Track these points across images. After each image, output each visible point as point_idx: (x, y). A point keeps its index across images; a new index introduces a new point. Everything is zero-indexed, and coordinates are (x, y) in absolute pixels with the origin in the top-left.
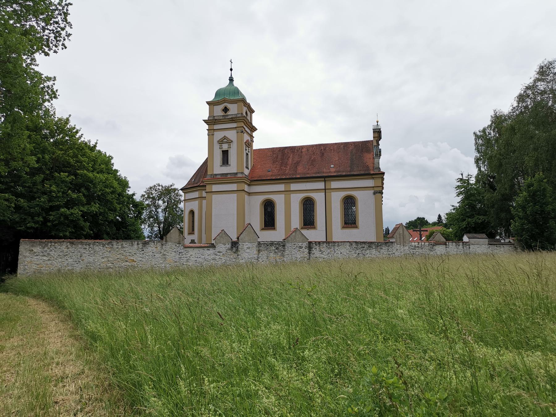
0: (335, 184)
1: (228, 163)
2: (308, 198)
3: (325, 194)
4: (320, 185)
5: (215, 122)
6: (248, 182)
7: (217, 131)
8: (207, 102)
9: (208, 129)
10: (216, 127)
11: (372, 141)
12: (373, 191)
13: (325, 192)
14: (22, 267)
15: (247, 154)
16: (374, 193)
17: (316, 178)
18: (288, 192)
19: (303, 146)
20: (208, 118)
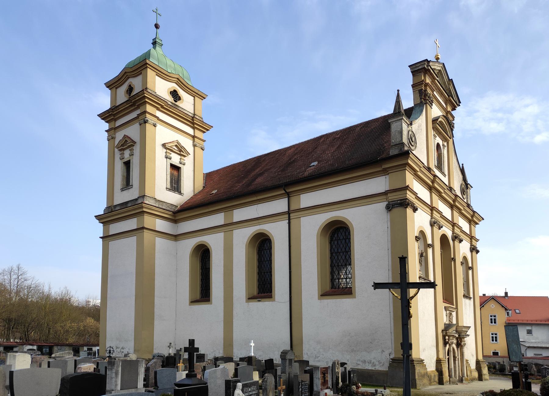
3: (289, 223)
5: (162, 107)
12: (385, 204)
13: (289, 220)
16: (389, 208)
18: (229, 226)
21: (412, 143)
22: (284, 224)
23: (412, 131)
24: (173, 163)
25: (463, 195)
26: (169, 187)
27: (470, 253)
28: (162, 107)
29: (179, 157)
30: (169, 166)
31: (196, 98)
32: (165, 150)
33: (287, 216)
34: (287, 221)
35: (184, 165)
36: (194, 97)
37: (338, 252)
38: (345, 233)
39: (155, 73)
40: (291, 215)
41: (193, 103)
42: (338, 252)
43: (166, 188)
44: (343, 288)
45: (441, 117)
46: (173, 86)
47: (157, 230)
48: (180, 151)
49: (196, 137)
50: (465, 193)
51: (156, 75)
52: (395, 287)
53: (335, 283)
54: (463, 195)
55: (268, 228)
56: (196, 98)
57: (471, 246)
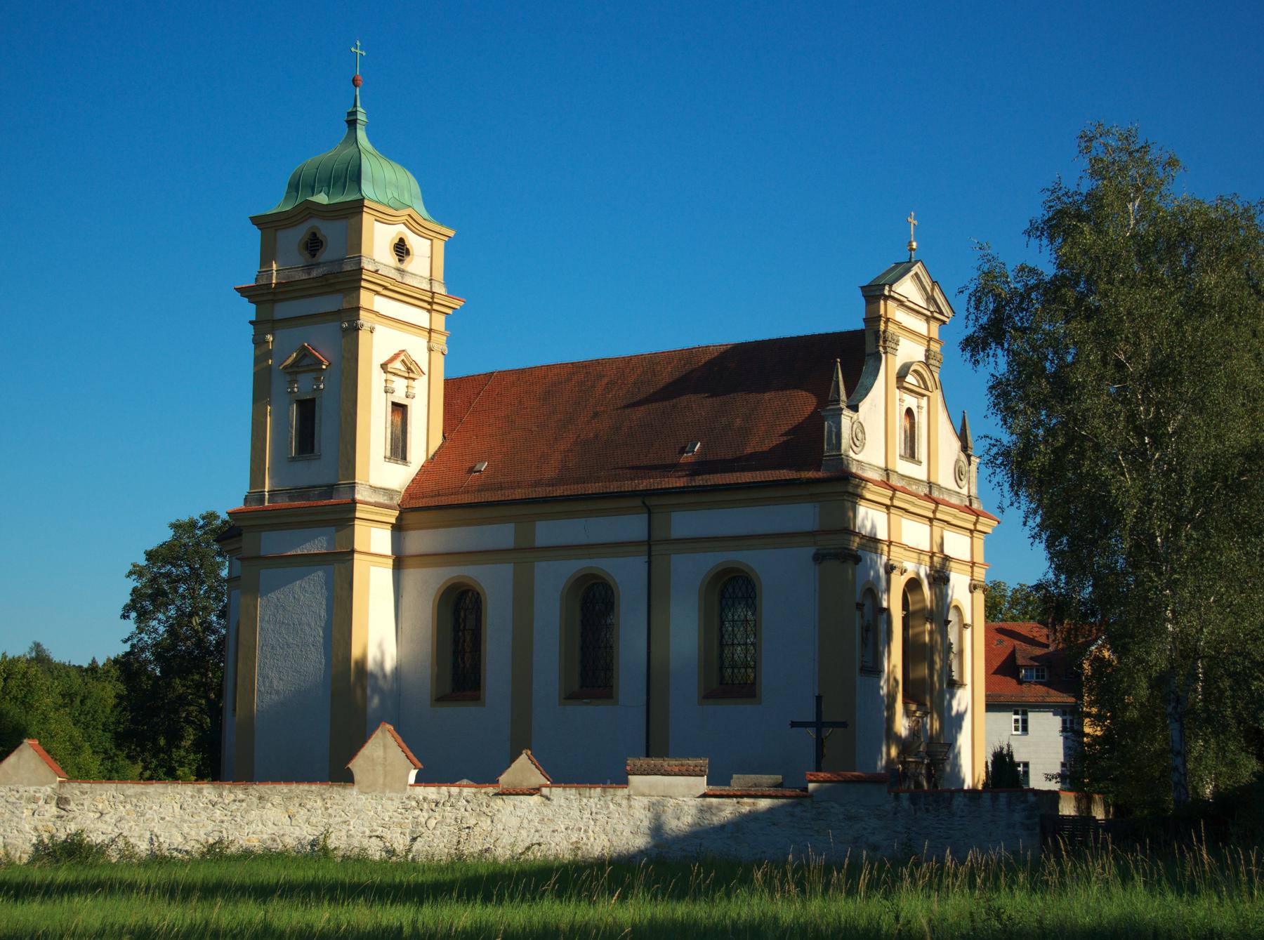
0: (684, 523)
1: (312, 450)
2: (594, 576)
3: (649, 563)
4: (632, 526)
5: (386, 288)
6: (885, 496)
7: (391, 327)
8: (252, 219)
9: (253, 318)
10: (284, 310)
11: (862, 331)
12: (811, 551)
13: (650, 556)
14: (129, 792)
15: (400, 409)
16: (819, 558)
17: (676, 493)
18: (524, 552)
19: (598, 362)
20: (256, 280)
21: (858, 443)
22: (639, 563)
23: (860, 422)
24: (396, 401)
25: (959, 481)
26: (388, 454)
27: (970, 595)
28: (386, 288)
29: (405, 382)
30: (390, 404)
31: (435, 240)
32: (384, 376)
33: (646, 548)
34: (646, 558)
35: (414, 397)
36: (431, 240)
37: (733, 621)
38: (747, 588)
39: (374, 218)
40: (653, 548)
41: (429, 254)
42: (733, 621)
43: (385, 457)
44: (740, 684)
45: (912, 369)
46: (399, 230)
47: (373, 551)
48: (409, 370)
49: (435, 331)
50: (962, 477)
51: (376, 220)
52: (850, 577)
53: (726, 674)
54: (959, 481)
55: (608, 566)
56: (435, 240)
57: (971, 580)
